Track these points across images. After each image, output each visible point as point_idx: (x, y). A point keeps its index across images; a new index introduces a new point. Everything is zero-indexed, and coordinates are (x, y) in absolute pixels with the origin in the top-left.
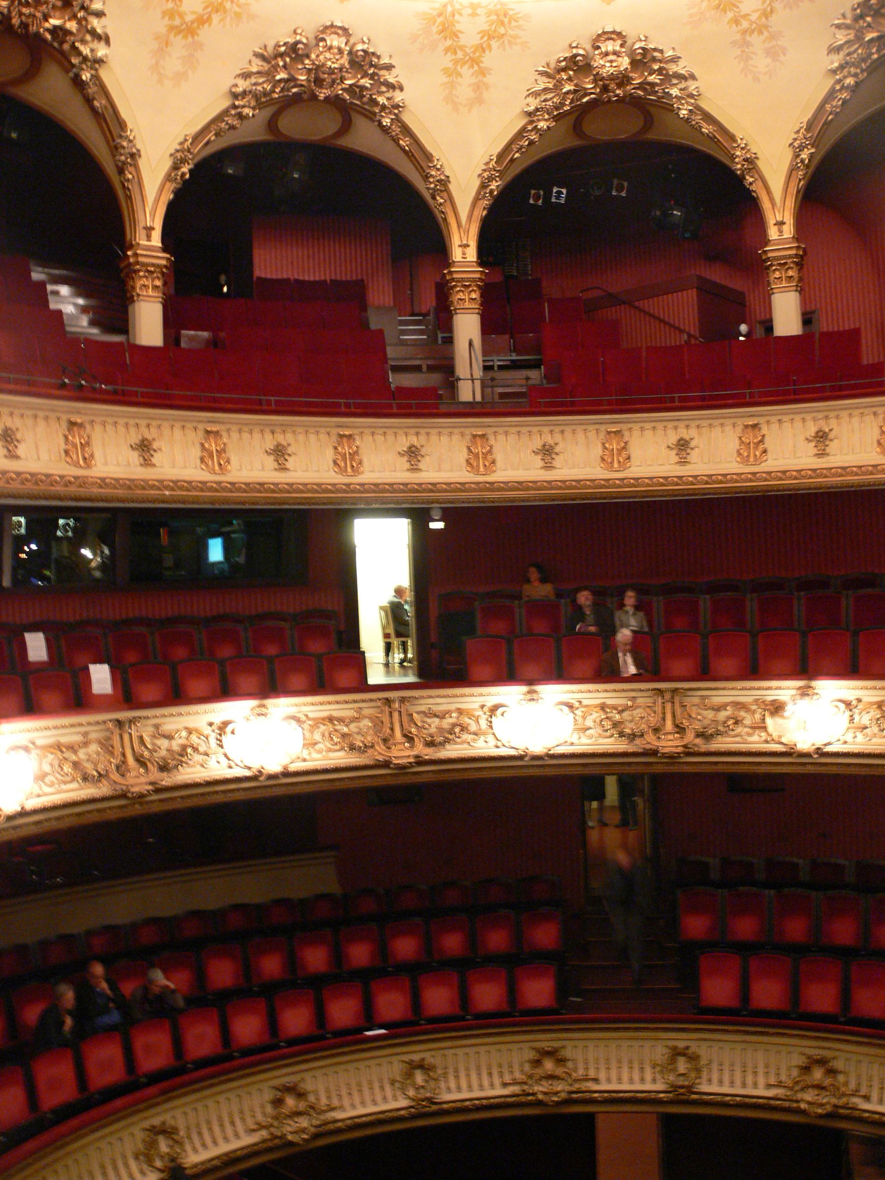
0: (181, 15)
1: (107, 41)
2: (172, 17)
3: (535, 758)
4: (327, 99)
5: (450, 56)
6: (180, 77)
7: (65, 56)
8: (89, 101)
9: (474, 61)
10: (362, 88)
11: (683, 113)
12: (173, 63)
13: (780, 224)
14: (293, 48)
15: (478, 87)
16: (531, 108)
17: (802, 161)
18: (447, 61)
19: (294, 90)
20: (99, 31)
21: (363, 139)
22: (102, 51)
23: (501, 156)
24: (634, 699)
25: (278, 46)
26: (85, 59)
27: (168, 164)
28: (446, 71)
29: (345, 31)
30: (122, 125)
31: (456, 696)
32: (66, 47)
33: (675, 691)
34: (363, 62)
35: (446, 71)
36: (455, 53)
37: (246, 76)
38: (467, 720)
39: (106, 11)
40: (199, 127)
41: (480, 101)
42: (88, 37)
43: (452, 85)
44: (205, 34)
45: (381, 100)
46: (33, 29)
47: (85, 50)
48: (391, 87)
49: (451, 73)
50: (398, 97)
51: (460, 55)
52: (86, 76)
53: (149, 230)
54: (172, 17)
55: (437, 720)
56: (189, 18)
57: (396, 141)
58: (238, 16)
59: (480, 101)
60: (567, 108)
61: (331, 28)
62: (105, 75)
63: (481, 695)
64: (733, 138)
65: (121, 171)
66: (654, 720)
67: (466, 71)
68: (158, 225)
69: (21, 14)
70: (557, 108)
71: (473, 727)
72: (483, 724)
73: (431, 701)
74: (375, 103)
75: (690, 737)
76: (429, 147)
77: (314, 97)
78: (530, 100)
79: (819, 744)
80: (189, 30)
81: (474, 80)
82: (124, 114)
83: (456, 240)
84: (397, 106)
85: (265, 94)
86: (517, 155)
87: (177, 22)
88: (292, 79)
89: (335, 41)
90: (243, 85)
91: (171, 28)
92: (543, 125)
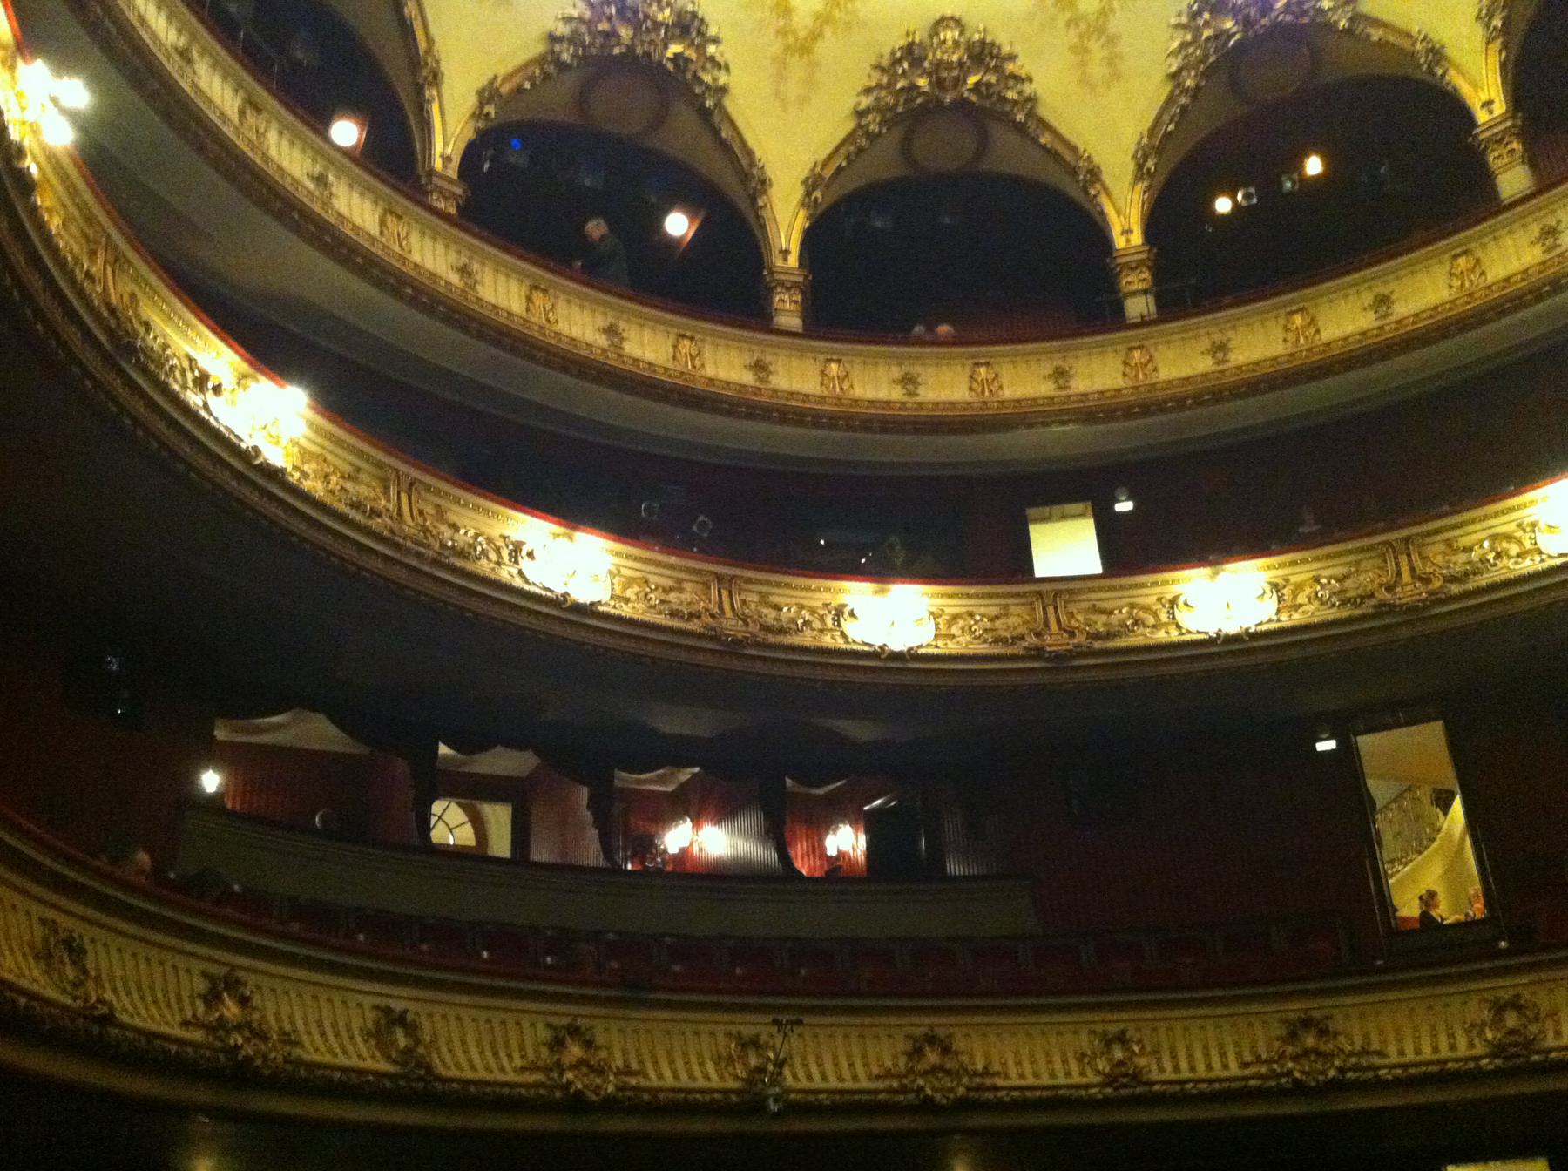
0: (794, 32)
1: (727, 68)
2: (785, 35)
3: (1235, 639)
4: (954, 103)
5: (1073, 32)
6: (803, 100)
7: (688, 88)
8: (716, 132)
9: (1101, 30)
10: (989, 85)
11: (1343, 24)
12: (793, 88)
13: (1488, 104)
14: (909, 49)
15: (1111, 61)
16: (1174, 69)
17: (1495, 28)
18: (1072, 37)
19: (919, 100)
20: (718, 58)
21: (1008, 156)
22: (723, 79)
23: (1152, 131)
24: (1357, 563)
25: (893, 53)
26: (708, 87)
27: (799, 192)
28: (1074, 49)
29: (957, 22)
30: (749, 153)
31: (1122, 588)
32: (689, 76)
33: (1407, 540)
34: (983, 53)
35: (1074, 49)
36: (1077, 25)
37: (867, 91)
38: (1141, 614)
39: (721, 36)
40: (828, 152)
41: (1116, 76)
42: (709, 66)
43: (1082, 65)
44: (821, 47)
45: (1011, 95)
46: (656, 57)
47: (707, 78)
48: (1018, 79)
49: (1080, 50)
50: (1028, 89)
51: (1083, 25)
52: (709, 103)
53: (785, 253)
54: (785, 35)
55: (1104, 618)
56: (802, 34)
57: (1035, 140)
58: (848, 26)
59: (1116, 76)
60: (1212, 59)
61: (942, 22)
62: (728, 104)
63: (1155, 584)
64: (1408, 35)
65: (753, 199)
66: (1388, 578)
67: (1095, 45)
68: (795, 248)
69: (643, 42)
70: (1202, 62)
71: (1151, 621)
72: (1164, 617)
73: (1093, 596)
74: (1004, 100)
75: (1437, 584)
76: (1073, 139)
77: (940, 103)
78: (1171, 60)
79: (914, 644)
80: (803, 47)
81: (1105, 52)
82: (751, 141)
83: (1116, 226)
84: (1029, 99)
85: (892, 108)
86: (1171, 127)
87: (791, 40)
88: (913, 87)
89: (950, 35)
90: (866, 102)
91: (787, 48)
92: (1189, 83)
